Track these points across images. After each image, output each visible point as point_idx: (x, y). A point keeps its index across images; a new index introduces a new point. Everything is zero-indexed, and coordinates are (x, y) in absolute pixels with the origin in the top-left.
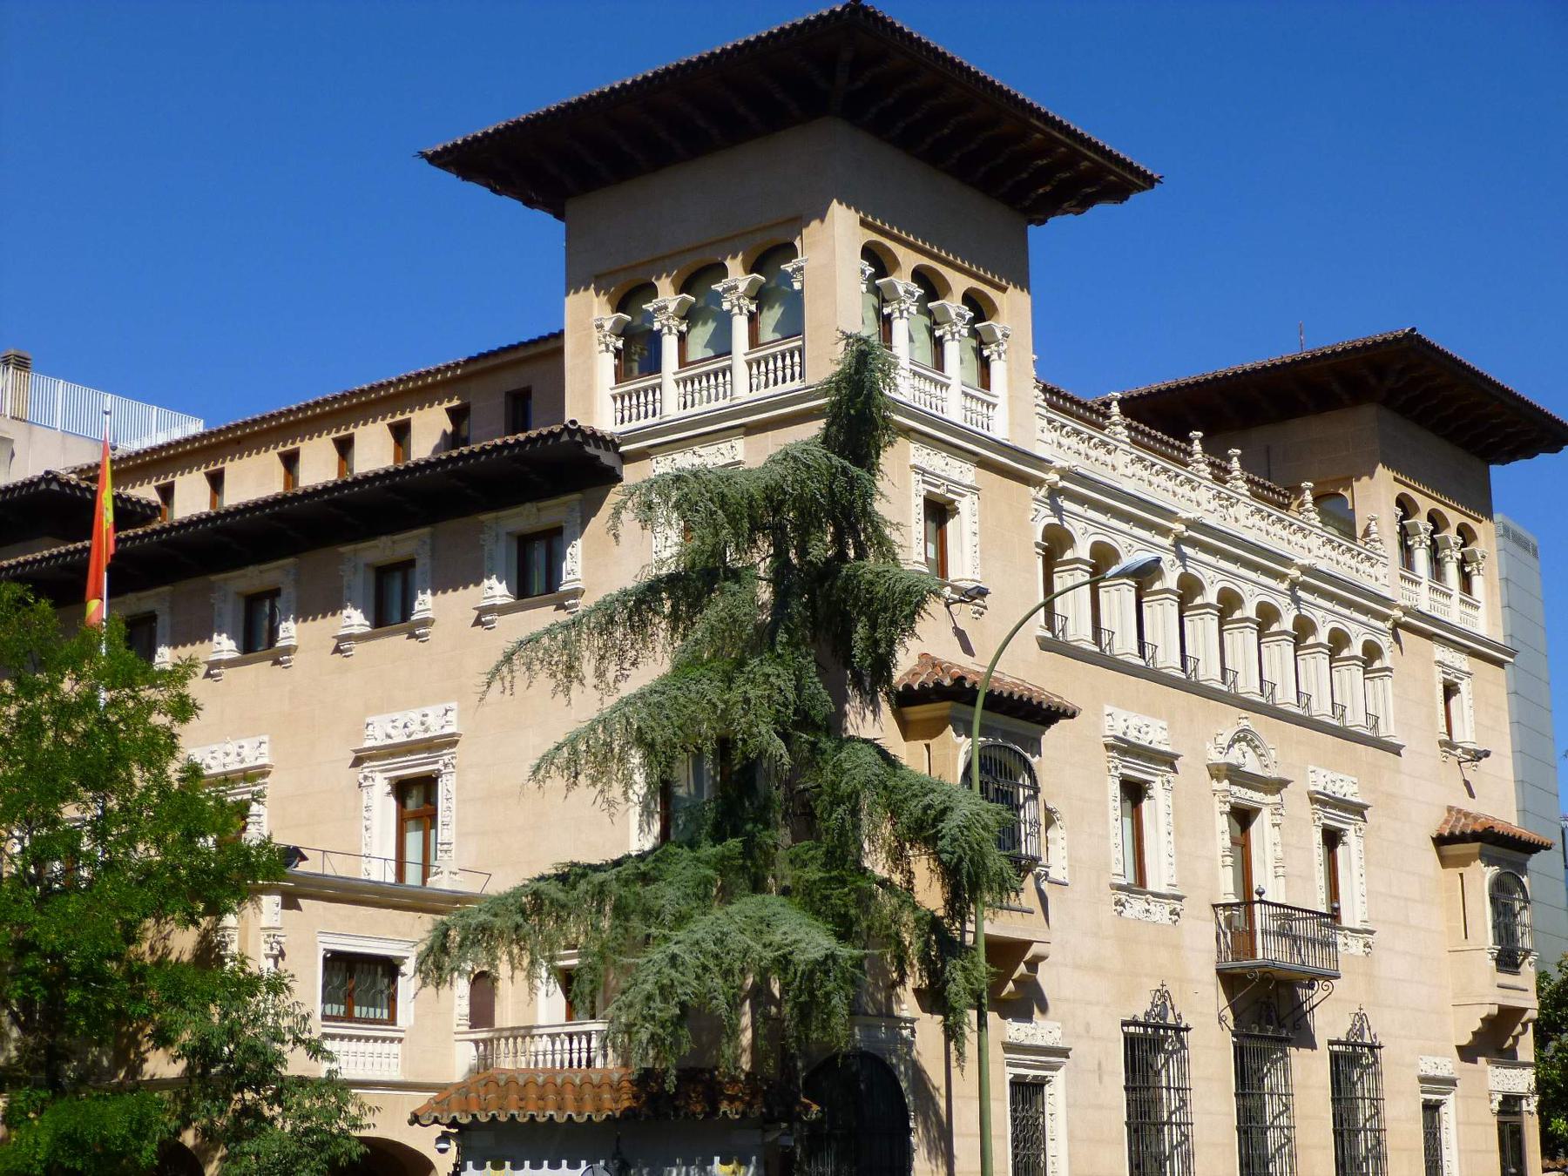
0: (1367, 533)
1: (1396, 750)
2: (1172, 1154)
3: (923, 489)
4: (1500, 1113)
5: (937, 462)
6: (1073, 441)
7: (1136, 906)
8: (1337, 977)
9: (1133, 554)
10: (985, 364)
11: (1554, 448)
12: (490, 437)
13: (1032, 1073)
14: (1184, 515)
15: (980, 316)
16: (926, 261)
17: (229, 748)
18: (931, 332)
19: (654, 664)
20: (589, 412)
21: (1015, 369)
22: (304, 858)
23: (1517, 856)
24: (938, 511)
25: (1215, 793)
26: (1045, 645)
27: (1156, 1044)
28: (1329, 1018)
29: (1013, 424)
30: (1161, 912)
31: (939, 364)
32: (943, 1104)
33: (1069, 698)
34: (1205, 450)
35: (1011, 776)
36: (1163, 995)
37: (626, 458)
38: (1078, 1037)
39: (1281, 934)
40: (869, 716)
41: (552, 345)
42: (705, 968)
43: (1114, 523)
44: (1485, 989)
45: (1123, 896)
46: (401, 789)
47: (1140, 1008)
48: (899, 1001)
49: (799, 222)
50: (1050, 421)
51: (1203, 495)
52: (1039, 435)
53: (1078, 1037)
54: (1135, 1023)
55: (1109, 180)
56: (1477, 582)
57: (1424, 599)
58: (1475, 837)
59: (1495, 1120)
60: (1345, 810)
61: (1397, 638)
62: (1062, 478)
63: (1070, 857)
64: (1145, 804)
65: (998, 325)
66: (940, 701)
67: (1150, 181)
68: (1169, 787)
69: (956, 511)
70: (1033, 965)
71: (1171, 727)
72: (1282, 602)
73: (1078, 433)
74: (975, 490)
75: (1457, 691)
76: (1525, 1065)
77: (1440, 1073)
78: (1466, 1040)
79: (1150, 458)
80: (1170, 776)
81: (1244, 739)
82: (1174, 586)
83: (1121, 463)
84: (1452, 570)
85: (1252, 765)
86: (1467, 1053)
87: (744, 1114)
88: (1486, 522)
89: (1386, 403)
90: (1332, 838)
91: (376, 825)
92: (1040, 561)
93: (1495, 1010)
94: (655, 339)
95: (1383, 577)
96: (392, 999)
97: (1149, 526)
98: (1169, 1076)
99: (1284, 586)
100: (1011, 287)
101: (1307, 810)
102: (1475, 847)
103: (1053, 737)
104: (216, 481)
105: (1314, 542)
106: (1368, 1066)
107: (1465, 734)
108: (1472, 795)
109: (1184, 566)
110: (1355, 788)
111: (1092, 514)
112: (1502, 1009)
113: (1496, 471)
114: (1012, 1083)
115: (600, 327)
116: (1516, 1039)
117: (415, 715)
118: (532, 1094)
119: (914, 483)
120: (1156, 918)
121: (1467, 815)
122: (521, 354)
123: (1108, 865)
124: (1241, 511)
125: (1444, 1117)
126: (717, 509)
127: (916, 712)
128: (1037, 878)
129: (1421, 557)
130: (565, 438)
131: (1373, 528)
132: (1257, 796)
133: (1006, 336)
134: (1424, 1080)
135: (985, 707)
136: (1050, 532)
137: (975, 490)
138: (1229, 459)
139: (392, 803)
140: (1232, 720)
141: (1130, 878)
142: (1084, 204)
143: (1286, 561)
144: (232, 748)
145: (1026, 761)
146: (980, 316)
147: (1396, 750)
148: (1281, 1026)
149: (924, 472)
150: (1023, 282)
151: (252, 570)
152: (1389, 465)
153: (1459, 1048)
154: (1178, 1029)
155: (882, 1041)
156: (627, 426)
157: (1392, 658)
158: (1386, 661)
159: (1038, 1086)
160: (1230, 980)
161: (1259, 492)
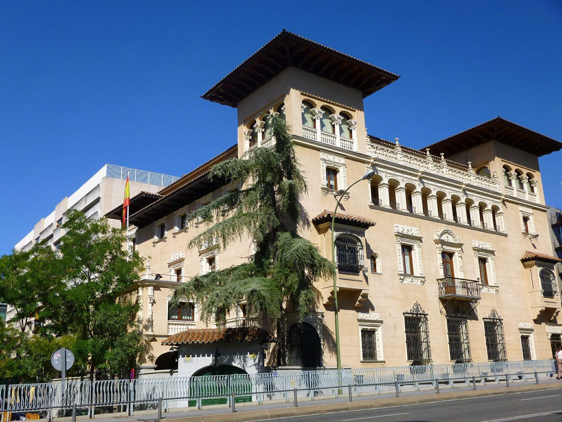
0: (494, 176)
1: (506, 235)
2: (465, 351)
3: (325, 165)
5: (330, 157)
6: (459, 174)
7: (408, 280)
8: (480, 299)
10: (351, 132)
11: (557, 149)
13: (369, 328)
14: (421, 170)
15: (530, 178)
16: (506, 163)
18: (331, 123)
22: (161, 277)
23: (551, 264)
24: (332, 172)
25: (437, 248)
27: (494, 324)
28: (483, 310)
30: (418, 282)
31: (510, 184)
32: (334, 337)
34: (430, 154)
35: (355, 243)
38: (386, 317)
39: (464, 287)
40: (306, 227)
42: (228, 297)
43: (397, 173)
45: (402, 277)
48: (318, 308)
49: (283, 96)
50: (372, 146)
53: (386, 317)
54: (407, 313)
55: (389, 79)
56: (535, 189)
58: (533, 259)
59: (550, 341)
60: (487, 252)
61: (505, 205)
62: (375, 161)
63: (383, 267)
64: (413, 252)
66: (322, 223)
67: (396, 78)
68: (492, 259)
69: (529, 219)
70: (557, 313)
71: (420, 230)
72: (461, 195)
73: (460, 172)
77: (529, 327)
79: (454, 169)
80: (493, 256)
81: (447, 233)
82: (491, 209)
83: (428, 165)
85: (451, 240)
86: (537, 321)
87: (252, 340)
88: (537, 172)
89: (497, 139)
90: (483, 261)
93: (544, 309)
94: (256, 134)
96: (193, 314)
97: (410, 174)
98: (498, 331)
99: (461, 190)
100: (357, 110)
102: (534, 262)
106: (499, 325)
108: (535, 248)
109: (424, 185)
110: (490, 246)
111: (453, 188)
114: (362, 331)
115: (245, 134)
116: (555, 317)
119: (322, 164)
121: (531, 253)
123: (397, 268)
124: (444, 170)
125: (530, 340)
128: (364, 271)
131: (495, 174)
132: (453, 249)
133: (355, 123)
134: (520, 329)
135: (335, 222)
139: (208, 264)
141: (403, 273)
143: (461, 183)
145: (358, 238)
146: (530, 178)
147: (506, 235)
148: (464, 313)
149: (325, 160)
150: (538, 170)
152: (499, 156)
153: (534, 320)
155: (310, 319)
158: (501, 210)
159: (527, 337)
160: (443, 300)
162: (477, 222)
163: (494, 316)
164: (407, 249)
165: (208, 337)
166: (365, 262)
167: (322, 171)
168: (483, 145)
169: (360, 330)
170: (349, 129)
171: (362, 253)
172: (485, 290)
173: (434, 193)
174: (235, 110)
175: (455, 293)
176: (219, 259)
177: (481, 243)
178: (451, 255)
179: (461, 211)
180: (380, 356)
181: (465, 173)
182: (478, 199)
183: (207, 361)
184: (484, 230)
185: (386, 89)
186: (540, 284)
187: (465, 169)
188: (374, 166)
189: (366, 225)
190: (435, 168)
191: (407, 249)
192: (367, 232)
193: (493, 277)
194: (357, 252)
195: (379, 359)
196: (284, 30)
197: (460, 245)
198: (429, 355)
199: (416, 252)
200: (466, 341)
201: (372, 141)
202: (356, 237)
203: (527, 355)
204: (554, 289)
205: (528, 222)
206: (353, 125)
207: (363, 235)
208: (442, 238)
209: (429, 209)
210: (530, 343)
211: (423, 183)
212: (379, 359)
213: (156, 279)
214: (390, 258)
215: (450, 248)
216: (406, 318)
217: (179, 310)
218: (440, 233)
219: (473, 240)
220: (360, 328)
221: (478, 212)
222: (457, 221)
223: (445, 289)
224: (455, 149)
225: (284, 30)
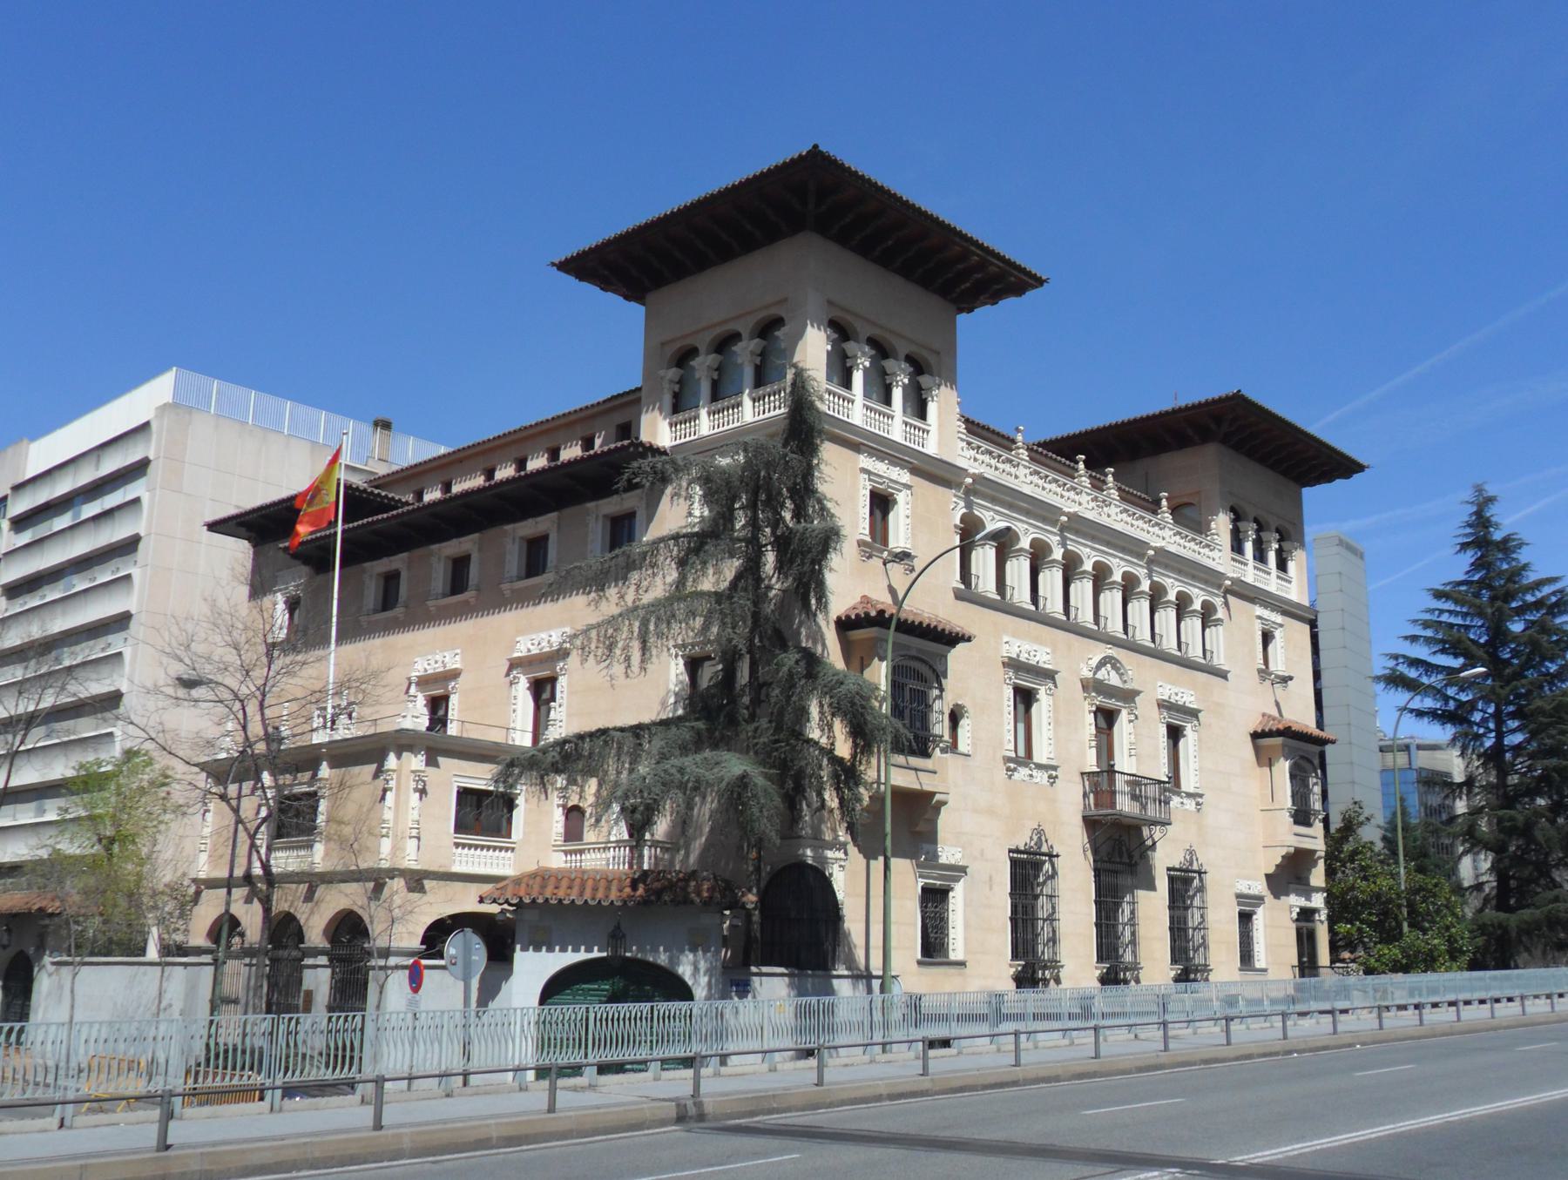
1: (1223, 675)
5: (881, 467)
6: (986, 458)
7: (1023, 772)
9: (993, 522)
17: (438, 657)
24: (881, 503)
26: (959, 596)
28: (1165, 856)
29: (940, 444)
30: (1041, 777)
34: (1087, 467)
36: (1039, 832)
44: (1288, 836)
47: (1022, 840)
50: (969, 443)
51: (1084, 498)
55: (1335, 466)
56: (1291, 565)
57: (1249, 574)
58: (1279, 733)
71: (1054, 651)
72: (1141, 572)
74: (908, 487)
75: (1273, 637)
76: (1317, 890)
79: (1044, 472)
83: (1024, 478)
85: (1114, 680)
89: (1224, 440)
90: (1175, 733)
95: (1219, 557)
102: (1279, 740)
103: (957, 658)
105: (1167, 533)
107: (1278, 666)
113: (1306, 491)
114: (923, 889)
117: (544, 635)
118: (564, 883)
123: (1001, 743)
134: (1239, 896)
137: (908, 487)
138: (1106, 475)
140: (1100, 651)
142: (995, 298)
147: (1223, 675)
154: (1200, 873)
160: (1090, 823)
161: (1125, 497)
162: (1052, 602)
163: (1039, 843)
164: (1025, 698)
165: (595, 889)
168: (1189, 450)
172: (1175, 801)
173: (1088, 566)
174: (636, 311)
175: (1113, 804)
176: (569, 684)
179: (1051, 580)
180: (956, 951)
181: (1005, 455)
184: (1038, 617)
185: (1009, 304)
186: (1289, 793)
187: (1153, 507)
188: (970, 492)
189: (952, 639)
191: (1025, 698)
196: (816, 147)
201: (969, 431)
203: (1246, 957)
208: (1099, 676)
213: (428, 729)
216: (1014, 862)
217: (483, 814)
218: (1094, 663)
219: (1158, 684)
220: (921, 882)
223: (1096, 799)
224: (1118, 452)
225: (816, 147)
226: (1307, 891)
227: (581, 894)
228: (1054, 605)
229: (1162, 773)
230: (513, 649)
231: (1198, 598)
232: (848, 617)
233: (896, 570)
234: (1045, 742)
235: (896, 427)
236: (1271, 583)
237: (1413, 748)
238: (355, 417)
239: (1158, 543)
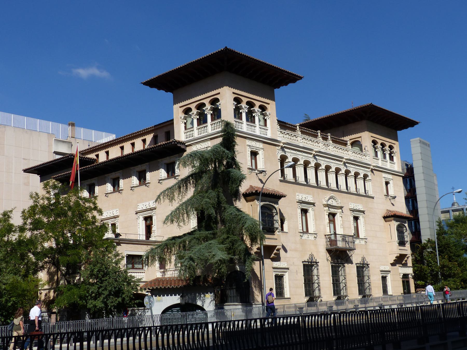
0: (365, 149)
2: (343, 289)
3: (250, 150)
4: (402, 278)
5: (253, 143)
6: (287, 136)
7: (305, 236)
10: (265, 121)
12: (162, 142)
13: (280, 273)
15: (391, 149)
19: (191, 192)
20: (179, 137)
21: (272, 122)
24: (254, 154)
27: (363, 267)
28: (356, 258)
29: (272, 133)
31: (376, 155)
33: (285, 193)
37: (187, 146)
38: (291, 265)
41: (172, 122)
43: (298, 153)
46: (146, 219)
47: (306, 258)
50: (281, 132)
52: (278, 135)
53: (291, 265)
57: (380, 163)
59: (401, 280)
61: (373, 172)
63: (288, 227)
64: (308, 214)
65: (268, 112)
66: (251, 195)
67: (301, 78)
69: (258, 154)
71: (313, 197)
76: (409, 267)
78: (392, 262)
83: (300, 139)
84: (388, 156)
85: (334, 203)
90: (356, 219)
91: (141, 227)
92: (279, 163)
93: (399, 255)
95: (368, 157)
98: (366, 273)
99: (342, 163)
101: (349, 213)
104: (107, 153)
112: (401, 255)
113: (398, 132)
116: (406, 261)
117: (147, 203)
120: (310, 239)
121: (390, 211)
122: (167, 123)
123: (298, 228)
124: (331, 147)
125: (388, 279)
126: (203, 158)
127: (249, 198)
129: (380, 154)
130: (173, 143)
134: (381, 271)
135: (262, 196)
136: (282, 156)
142: (286, 84)
143: (342, 158)
144: (111, 212)
151: (113, 173)
156: (187, 139)
157: (371, 177)
160: (329, 251)
164: (304, 212)
166: (277, 225)
167: (248, 155)
169: (274, 275)
170: (264, 118)
171: (277, 218)
172: (357, 242)
175: (337, 244)
177: (355, 205)
178: (334, 215)
179: (311, 172)
180: (287, 293)
182: (354, 169)
183: (175, 299)
188: (282, 148)
190: (324, 146)
191: (304, 212)
192: (281, 201)
193: (363, 232)
194: (404, 233)
195: (286, 296)
197: (341, 208)
198: (320, 293)
199: (310, 215)
200: (344, 281)
202: (272, 205)
204: (406, 239)
205: (389, 185)
206: (267, 115)
207: (277, 203)
209: (285, 173)
210: (387, 281)
211: (346, 166)
212: (286, 296)
214: (293, 221)
215: (334, 210)
216: (304, 265)
218: (327, 199)
221: (324, 173)
222: (284, 178)
226: (405, 265)
227: (159, 285)
228: (312, 181)
229: (352, 232)
230: (137, 208)
231: (362, 173)
232: (246, 193)
233: (261, 176)
234: (312, 226)
235: (257, 131)
236: (388, 165)
237: (451, 211)
238: (62, 123)
239: (348, 157)
